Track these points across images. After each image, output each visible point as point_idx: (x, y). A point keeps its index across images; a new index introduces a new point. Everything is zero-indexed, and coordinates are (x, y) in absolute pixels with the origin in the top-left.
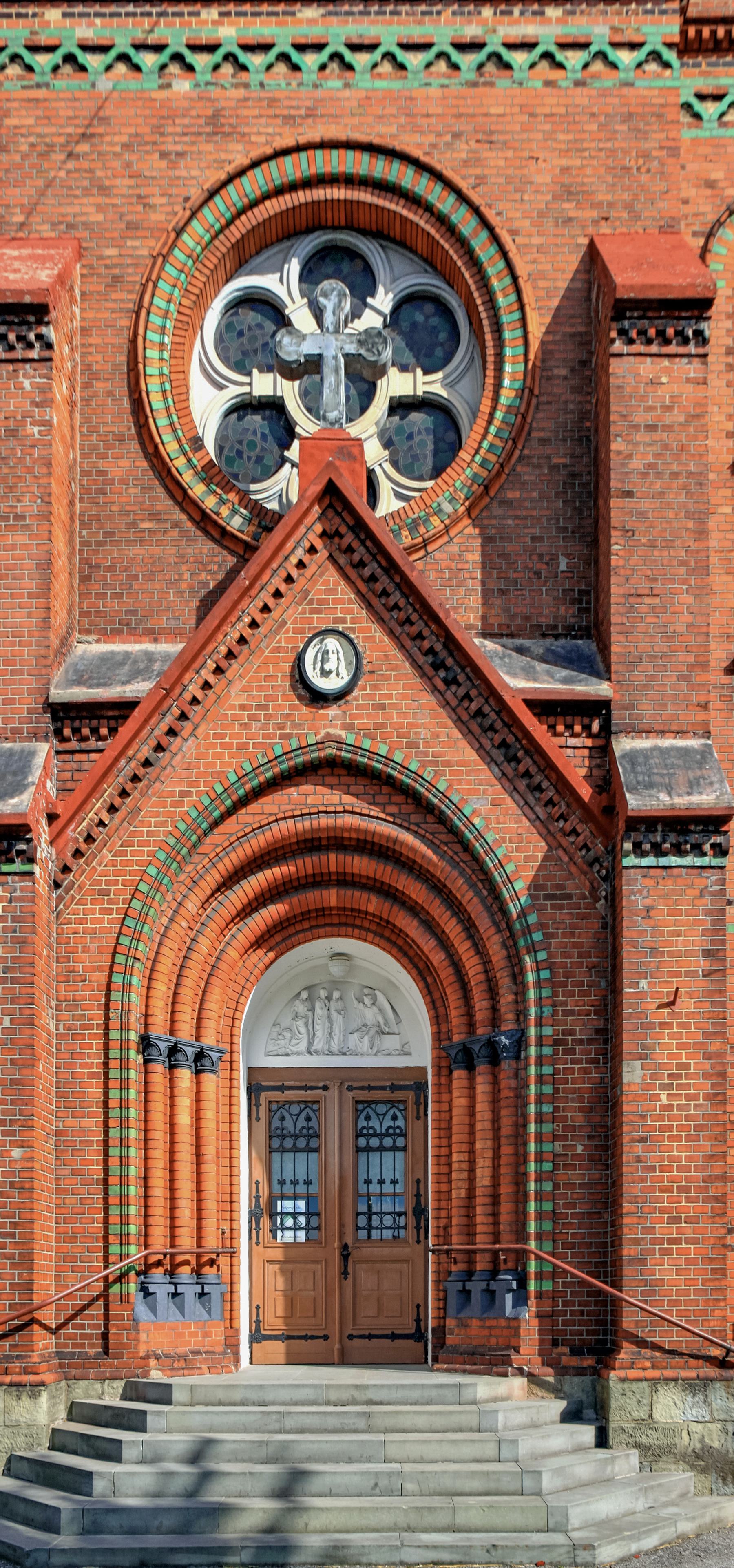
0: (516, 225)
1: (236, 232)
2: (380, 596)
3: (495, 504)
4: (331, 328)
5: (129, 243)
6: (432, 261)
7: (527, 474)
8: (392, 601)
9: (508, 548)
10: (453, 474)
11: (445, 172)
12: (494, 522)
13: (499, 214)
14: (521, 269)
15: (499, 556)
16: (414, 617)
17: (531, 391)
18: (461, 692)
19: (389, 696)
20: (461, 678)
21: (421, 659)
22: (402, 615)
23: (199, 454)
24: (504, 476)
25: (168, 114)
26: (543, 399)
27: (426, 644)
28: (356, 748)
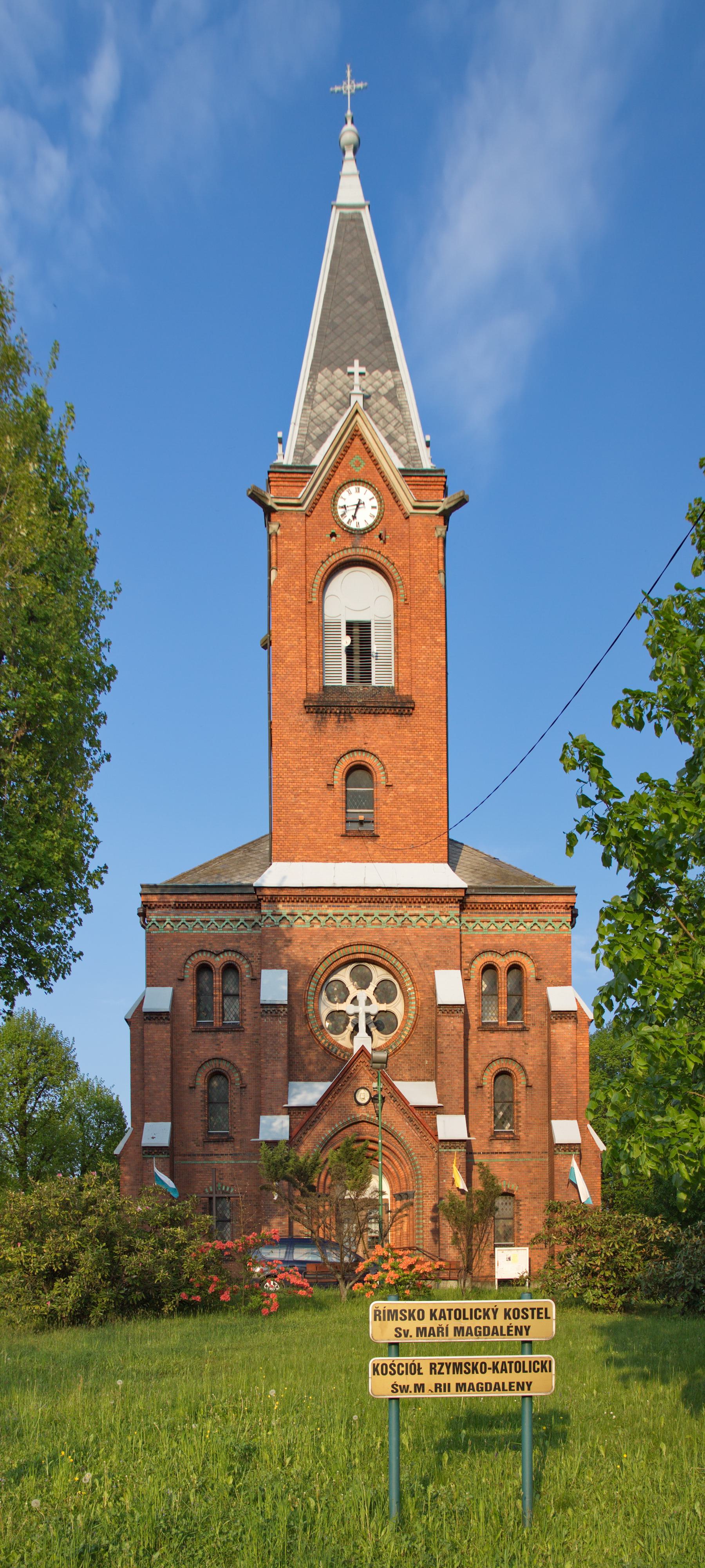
7: (416, 1037)
9: (411, 1058)
25: (313, 934)
28: (370, 1119)
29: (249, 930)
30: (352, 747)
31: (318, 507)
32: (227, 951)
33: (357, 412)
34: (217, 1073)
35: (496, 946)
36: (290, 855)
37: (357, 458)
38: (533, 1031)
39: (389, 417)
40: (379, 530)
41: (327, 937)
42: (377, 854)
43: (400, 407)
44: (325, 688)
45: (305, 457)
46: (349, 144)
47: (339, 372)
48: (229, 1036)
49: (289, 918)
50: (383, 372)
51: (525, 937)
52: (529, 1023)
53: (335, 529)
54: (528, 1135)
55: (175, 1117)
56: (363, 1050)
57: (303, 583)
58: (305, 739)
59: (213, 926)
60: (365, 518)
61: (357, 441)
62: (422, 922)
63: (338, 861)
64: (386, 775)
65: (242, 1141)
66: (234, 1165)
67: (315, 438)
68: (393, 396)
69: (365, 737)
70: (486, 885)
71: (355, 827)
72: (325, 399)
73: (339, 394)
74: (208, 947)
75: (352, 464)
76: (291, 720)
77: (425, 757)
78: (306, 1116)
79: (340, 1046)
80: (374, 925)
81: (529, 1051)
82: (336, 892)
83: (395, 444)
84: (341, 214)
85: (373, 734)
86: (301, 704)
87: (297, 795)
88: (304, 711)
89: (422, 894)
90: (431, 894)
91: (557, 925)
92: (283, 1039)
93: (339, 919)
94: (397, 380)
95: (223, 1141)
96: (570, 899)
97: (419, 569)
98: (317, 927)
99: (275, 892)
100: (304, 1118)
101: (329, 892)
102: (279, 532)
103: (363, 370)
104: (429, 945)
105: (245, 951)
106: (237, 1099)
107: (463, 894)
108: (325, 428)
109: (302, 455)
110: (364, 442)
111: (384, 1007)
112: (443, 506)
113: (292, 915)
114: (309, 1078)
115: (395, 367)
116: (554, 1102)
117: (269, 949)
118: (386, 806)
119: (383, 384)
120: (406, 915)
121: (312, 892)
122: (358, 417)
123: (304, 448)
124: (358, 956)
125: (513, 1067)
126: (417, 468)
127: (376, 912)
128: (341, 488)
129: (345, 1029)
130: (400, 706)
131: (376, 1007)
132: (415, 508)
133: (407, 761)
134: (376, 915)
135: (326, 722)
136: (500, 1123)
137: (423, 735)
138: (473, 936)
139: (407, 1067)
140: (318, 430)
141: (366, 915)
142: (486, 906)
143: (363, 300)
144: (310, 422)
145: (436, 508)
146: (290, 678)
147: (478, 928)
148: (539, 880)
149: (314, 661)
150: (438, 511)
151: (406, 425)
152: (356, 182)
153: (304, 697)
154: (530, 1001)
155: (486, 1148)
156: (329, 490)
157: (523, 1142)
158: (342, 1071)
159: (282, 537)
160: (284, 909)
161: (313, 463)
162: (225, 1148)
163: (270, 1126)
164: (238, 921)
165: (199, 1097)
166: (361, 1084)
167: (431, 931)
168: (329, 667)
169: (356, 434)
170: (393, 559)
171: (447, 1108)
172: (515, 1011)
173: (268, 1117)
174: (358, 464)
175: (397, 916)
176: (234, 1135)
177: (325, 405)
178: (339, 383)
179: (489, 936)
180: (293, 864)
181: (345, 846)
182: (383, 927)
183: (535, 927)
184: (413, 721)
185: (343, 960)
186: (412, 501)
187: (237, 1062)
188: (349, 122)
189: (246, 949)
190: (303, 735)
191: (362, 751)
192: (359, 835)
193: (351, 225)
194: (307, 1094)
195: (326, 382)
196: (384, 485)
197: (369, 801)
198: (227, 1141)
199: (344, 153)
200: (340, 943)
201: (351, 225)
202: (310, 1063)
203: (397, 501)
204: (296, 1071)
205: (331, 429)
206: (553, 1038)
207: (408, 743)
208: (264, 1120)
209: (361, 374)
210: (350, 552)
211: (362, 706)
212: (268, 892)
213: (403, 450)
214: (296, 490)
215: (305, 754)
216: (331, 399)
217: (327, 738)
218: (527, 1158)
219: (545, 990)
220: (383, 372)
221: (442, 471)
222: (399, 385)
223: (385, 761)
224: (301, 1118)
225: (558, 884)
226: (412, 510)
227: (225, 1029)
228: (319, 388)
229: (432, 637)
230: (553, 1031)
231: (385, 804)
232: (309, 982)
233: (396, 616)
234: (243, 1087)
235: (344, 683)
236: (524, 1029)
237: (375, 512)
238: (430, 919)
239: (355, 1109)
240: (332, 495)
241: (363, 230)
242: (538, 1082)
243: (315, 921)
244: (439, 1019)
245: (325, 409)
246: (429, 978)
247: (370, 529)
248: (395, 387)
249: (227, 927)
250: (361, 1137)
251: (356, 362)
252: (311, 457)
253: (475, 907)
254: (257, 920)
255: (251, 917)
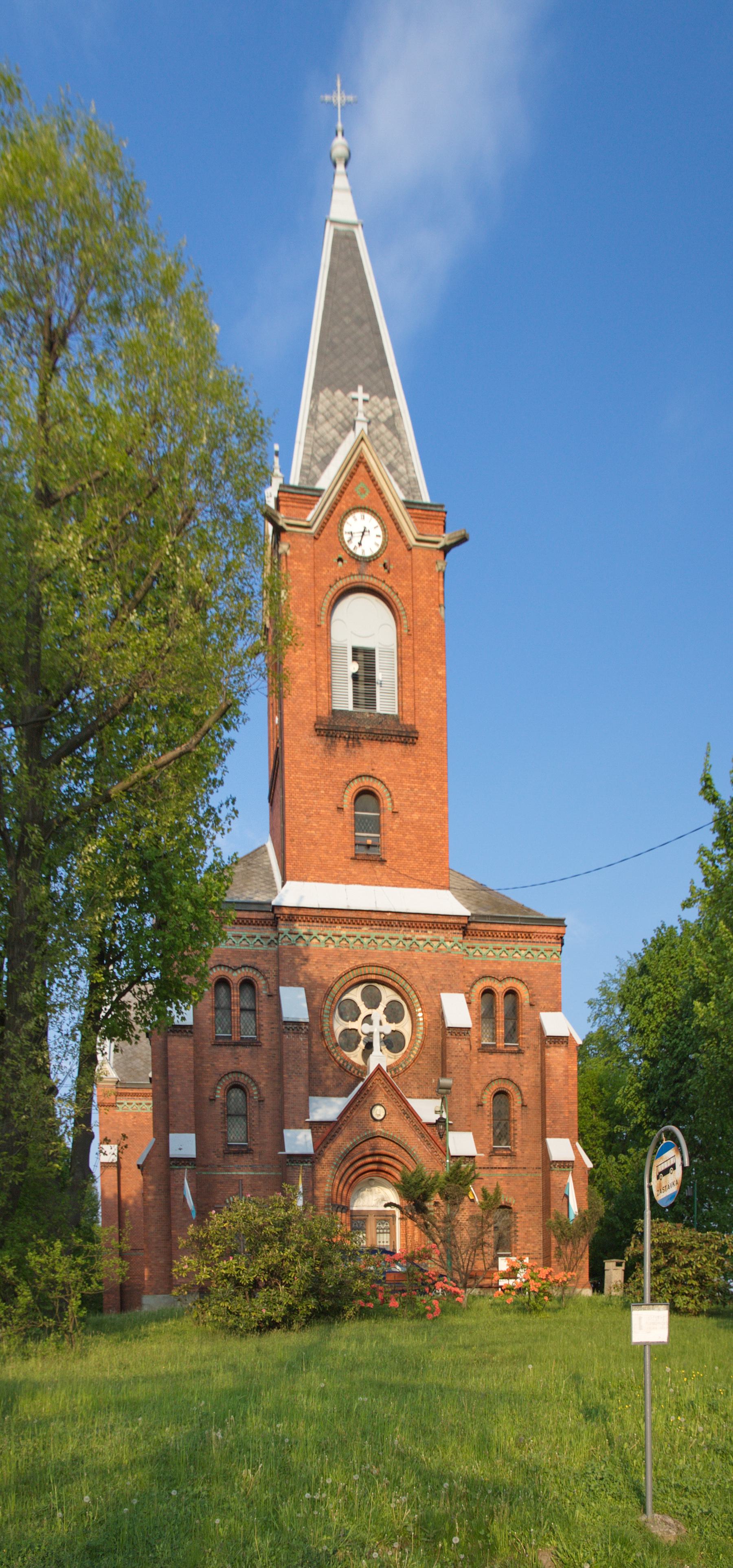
6: (398, 992)
25: (328, 954)
29: (265, 947)
30: (361, 771)
31: (325, 531)
32: (244, 966)
33: (362, 439)
34: (236, 1086)
35: (494, 972)
36: (303, 875)
37: (362, 485)
38: (527, 1054)
39: (389, 445)
40: (384, 559)
41: (341, 958)
42: (385, 878)
43: (398, 436)
44: (334, 712)
45: (311, 478)
46: (340, 158)
47: (339, 393)
48: (248, 1050)
49: (306, 937)
50: (382, 399)
51: (520, 964)
52: (523, 1045)
53: (341, 555)
54: (525, 1151)
55: (198, 1129)
56: (379, 1068)
57: (313, 605)
58: (316, 761)
59: (230, 942)
60: (370, 546)
61: (362, 468)
62: (428, 946)
63: (348, 883)
64: (392, 801)
65: (260, 1153)
66: (253, 1177)
67: (319, 459)
68: (392, 424)
69: (372, 763)
70: (483, 912)
71: (363, 851)
72: (327, 420)
73: (340, 417)
74: (226, 962)
75: (358, 490)
76: (303, 741)
77: (428, 786)
78: (328, 1129)
79: (353, 1064)
80: (387, 947)
81: (525, 1073)
82: (350, 914)
83: (395, 473)
84: (335, 230)
85: (380, 761)
86: (311, 727)
87: (309, 816)
88: (314, 733)
89: (429, 919)
90: (437, 920)
91: (548, 954)
92: (304, 1054)
93: (351, 940)
94: (395, 408)
95: (243, 1152)
96: (560, 930)
97: (421, 602)
98: (332, 947)
99: (294, 912)
100: (325, 1132)
101: (343, 914)
102: (289, 553)
103: (367, 397)
104: (435, 969)
105: (261, 968)
106: (256, 1112)
107: (465, 921)
108: (329, 450)
109: (307, 476)
110: (367, 467)
111: (393, 1026)
112: (444, 541)
113: (310, 934)
114: (326, 1094)
115: (393, 395)
116: (548, 1121)
117: (286, 966)
118: (392, 833)
119: (382, 411)
120: (414, 939)
121: (327, 913)
122: (363, 444)
123: (309, 468)
124: (369, 977)
125: (510, 1088)
126: (417, 500)
127: (387, 935)
128: (347, 514)
129: (356, 1047)
130: (407, 737)
131: (388, 1028)
132: (417, 540)
133: (412, 789)
134: (386, 938)
135: (336, 746)
136: (498, 1139)
137: (426, 765)
138: (473, 962)
139: (415, 1085)
140: (322, 452)
141: (377, 938)
142: (485, 934)
143: (360, 322)
144: (315, 442)
145: (437, 543)
146: (301, 700)
147: (477, 954)
148: (529, 910)
149: (323, 685)
150: (439, 546)
151: (404, 454)
152: (348, 198)
153: (314, 719)
154: (525, 1025)
155: (486, 1164)
156: (336, 516)
157: (518, 1159)
158: (360, 1087)
159: (291, 557)
160: (301, 928)
161: (319, 485)
162: (245, 1160)
163: (295, 1139)
164: (254, 937)
165: (218, 1109)
166: (377, 1101)
167: (437, 956)
168: (337, 690)
169: (361, 461)
170: (396, 589)
171: (455, 1126)
172: (512, 1034)
173: (292, 1131)
174: (363, 491)
175: (405, 939)
176: (253, 1147)
177: (327, 426)
178: (340, 405)
179: (488, 962)
180: (307, 884)
181: (355, 869)
182: (393, 949)
183: (529, 956)
184: (416, 750)
185: (356, 980)
186: (415, 533)
187: (255, 1076)
188: (340, 134)
189: (263, 966)
190: (314, 757)
191: (370, 776)
192: (367, 859)
193: (345, 243)
194: (327, 1109)
195: (328, 403)
196: (387, 515)
197: (376, 825)
198: (246, 1153)
199: (335, 165)
200: (353, 963)
201: (345, 243)
202: (328, 1078)
203: (400, 532)
204: (318, 1087)
205: (334, 452)
206: (548, 1061)
207: (412, 771)
208: (288, 1133)
209: (365, 401)
210: (356, 578)
211: (370, 732)
212: (286, 911)
213: (404, 480)
214: (304, 511)
215: (316, 776)
216: (333, 421)
217: (337, 762)
218: (523, 1173)
219: (538, 1015)
220: (382, 399)
221: (442, 506)
222: (396, 414)
223: (391, 788)
224: (323, 1132)
225: (548, 915)
226: (414, 543)
227: (243, 1043)
228: (321, 408)
229: (434, 670)
230: (547, 1054)
231: (392, 829)
232: (325, 999)
233: (399, 645)
234: (261, 1101)
235: (350, 708)
236: (520, 1052)
237: (380, 541)
238: (435, 944)
239: (372, 1123)
240: (338, 520)
241: (356, 249)
242: (533, 1102)
243: (330, 941)
244: (448, 1041)
245: (327, 430)
246: (436, 1001)
247: (374, 558)
248: (394, 415)
249: (244, 943)
250: (377, 1151)
251: (360, 388)
252: (316, 479)
253: (476, 934)
254: (272, 938)
255: (267, 934)
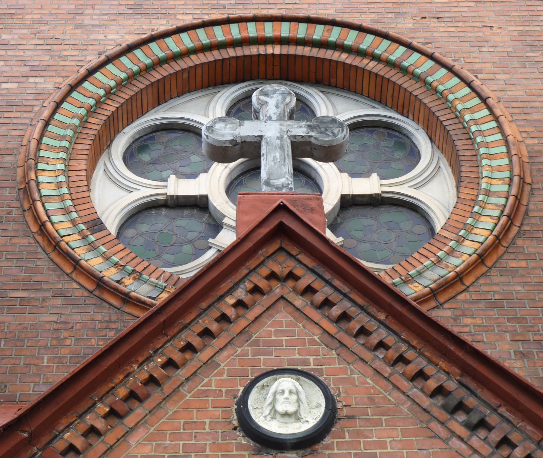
0: (477, 66)
1: (156, 76)
2: (356, 336)
3: (493, 272)
4: (274, 117)
5: (31, 80)
8: (374, 339)
10: (434, 249)
11: (129, 42)
12: (495, 288)
13: (455, 60)
14: (486, 91)
15: (509, 320)
16: (410, 354)
17: (522, 179)
18: (495, 436)
19: (383, 445)
20: (492, 419)
21: (426, 402)
22: (392, 354)
23: (99, 235)
24: (501, 250)
26: (534, 186)
27: (432, 384)
